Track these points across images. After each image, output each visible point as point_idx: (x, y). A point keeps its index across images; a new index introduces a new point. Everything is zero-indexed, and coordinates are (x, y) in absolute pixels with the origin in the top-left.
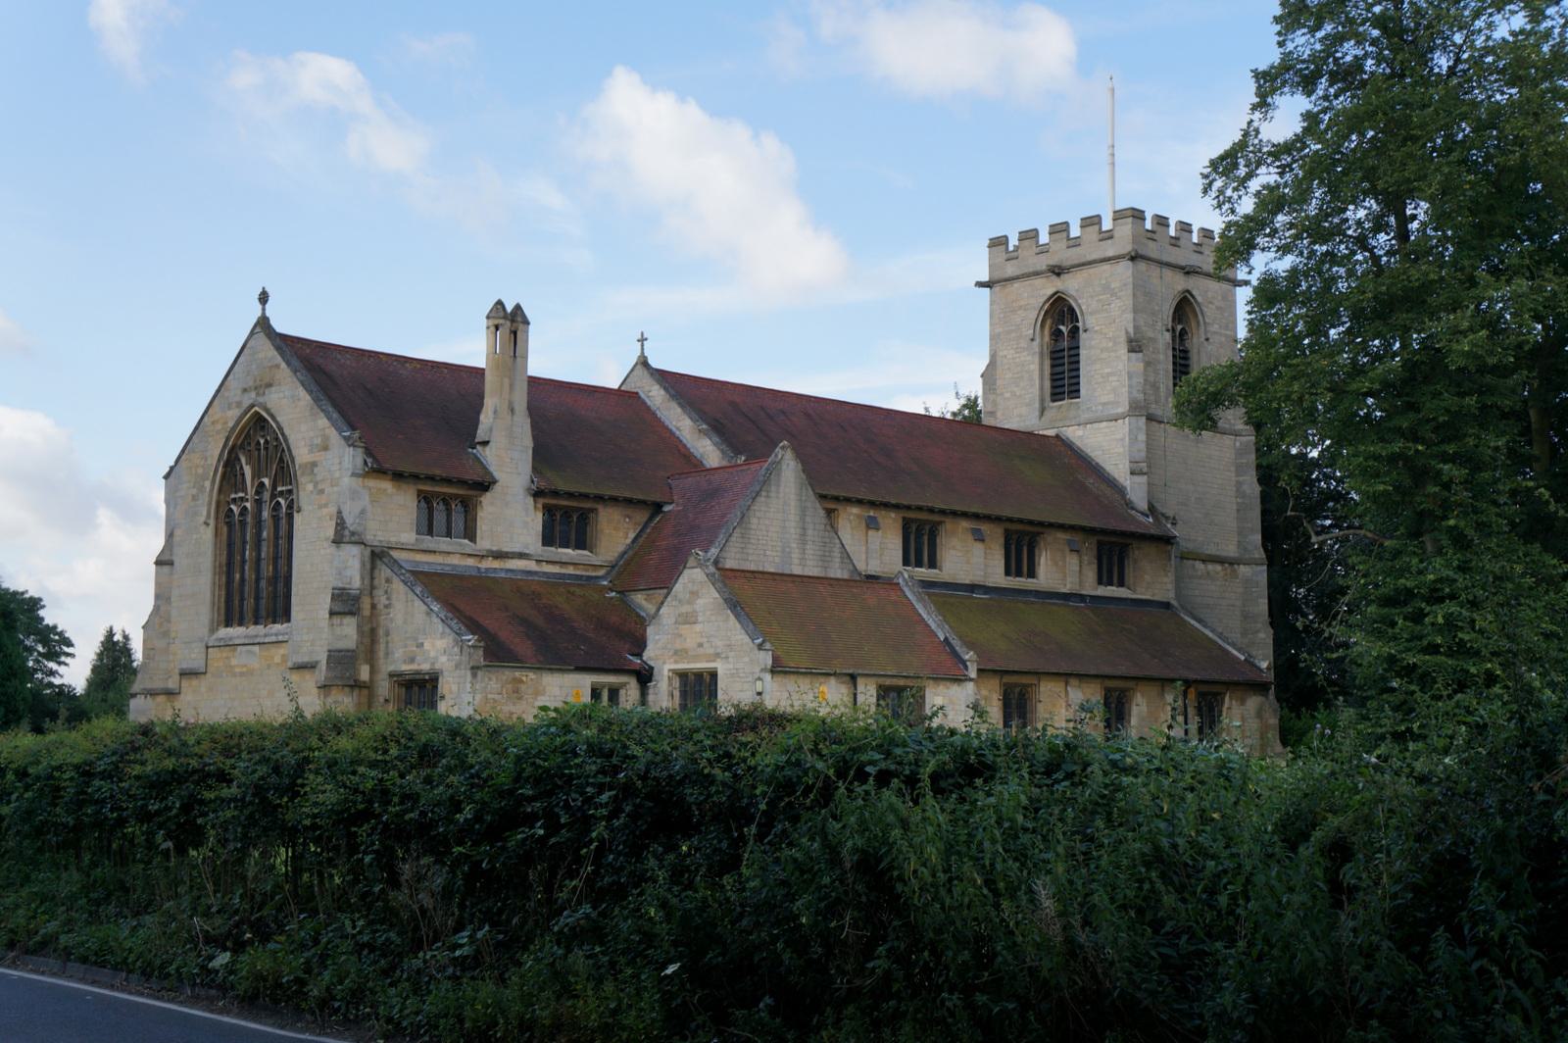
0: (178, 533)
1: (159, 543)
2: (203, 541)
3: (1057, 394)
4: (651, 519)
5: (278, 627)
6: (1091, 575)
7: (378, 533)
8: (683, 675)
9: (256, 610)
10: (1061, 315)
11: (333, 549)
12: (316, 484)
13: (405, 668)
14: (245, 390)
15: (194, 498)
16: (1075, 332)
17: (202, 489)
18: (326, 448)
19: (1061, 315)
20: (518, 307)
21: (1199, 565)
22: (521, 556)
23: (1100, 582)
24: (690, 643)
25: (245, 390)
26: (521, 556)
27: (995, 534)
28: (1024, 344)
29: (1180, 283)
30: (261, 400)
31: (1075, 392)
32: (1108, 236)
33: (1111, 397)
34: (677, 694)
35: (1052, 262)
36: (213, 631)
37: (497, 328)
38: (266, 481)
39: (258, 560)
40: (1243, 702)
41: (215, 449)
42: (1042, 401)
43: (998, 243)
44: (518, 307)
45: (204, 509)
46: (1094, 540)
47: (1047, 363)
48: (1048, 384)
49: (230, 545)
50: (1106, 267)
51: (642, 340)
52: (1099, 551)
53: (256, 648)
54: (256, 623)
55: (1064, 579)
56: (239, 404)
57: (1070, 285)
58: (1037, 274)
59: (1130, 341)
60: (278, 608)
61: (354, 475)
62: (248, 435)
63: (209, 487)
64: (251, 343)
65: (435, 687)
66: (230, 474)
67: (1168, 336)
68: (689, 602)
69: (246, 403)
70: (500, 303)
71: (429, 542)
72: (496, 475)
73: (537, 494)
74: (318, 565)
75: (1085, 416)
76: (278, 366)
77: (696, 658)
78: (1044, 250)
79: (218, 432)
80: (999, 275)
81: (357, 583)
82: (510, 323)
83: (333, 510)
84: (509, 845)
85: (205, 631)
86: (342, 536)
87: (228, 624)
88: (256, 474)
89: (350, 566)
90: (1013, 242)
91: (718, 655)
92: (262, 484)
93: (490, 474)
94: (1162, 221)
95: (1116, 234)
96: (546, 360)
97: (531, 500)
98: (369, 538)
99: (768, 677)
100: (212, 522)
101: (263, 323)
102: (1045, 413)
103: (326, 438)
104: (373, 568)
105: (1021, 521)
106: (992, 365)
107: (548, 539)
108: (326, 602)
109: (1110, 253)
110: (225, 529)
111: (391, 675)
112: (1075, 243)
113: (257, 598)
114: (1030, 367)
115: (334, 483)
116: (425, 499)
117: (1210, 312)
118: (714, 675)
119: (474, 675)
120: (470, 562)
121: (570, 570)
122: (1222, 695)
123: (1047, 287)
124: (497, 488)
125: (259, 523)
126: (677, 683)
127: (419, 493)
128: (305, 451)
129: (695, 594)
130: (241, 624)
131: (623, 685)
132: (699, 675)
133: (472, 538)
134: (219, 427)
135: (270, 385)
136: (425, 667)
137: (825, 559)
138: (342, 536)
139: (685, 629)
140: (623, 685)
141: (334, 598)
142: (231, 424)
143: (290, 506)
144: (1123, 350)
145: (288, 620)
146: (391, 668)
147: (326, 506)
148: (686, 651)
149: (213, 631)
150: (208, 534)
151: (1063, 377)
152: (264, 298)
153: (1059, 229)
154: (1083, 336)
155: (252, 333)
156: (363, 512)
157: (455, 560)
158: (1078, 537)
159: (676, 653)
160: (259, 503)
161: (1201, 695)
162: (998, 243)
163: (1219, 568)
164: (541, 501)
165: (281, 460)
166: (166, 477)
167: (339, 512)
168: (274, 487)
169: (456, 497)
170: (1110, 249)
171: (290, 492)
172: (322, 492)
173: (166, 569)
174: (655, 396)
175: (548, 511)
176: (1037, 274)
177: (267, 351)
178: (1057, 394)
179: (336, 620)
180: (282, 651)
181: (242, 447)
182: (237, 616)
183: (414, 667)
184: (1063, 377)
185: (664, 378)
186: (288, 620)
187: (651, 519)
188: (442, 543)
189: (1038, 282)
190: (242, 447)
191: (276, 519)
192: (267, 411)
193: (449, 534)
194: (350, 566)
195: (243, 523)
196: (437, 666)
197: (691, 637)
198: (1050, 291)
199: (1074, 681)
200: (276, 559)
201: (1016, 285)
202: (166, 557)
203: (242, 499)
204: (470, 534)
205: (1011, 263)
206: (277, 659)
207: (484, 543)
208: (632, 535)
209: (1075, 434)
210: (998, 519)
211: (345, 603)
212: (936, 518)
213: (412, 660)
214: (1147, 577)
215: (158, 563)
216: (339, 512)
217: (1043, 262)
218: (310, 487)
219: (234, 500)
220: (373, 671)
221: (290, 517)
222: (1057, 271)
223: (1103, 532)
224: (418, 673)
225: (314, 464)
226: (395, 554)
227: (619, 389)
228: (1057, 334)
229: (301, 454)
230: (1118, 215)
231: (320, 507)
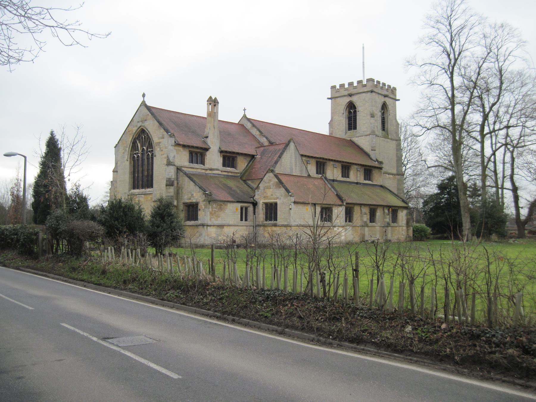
0: (119, 163)
1: (113, 166)
2: (127, 165)
3: (350, 129)
4: (251, 160)
5: (149, 189)
6: (362, 177)
7: (178, 163)
8: (266, 204)
9: (142, 184)
10: (351, 108)
11: (166, 167)
12: (160, 148)
13: (188, 201)
14: (138, 122)
15: (124, 153)
16: (355, 112)
17: (126, 150)
18: (163, 138)
19: (351, 108)
20: (216, 98)
21: (387, 175)
22: (217, 170)
23: (365, 179)
24: (269, 194)
25: (138, 122)
26: (217, 170)
27: (339, 166)
28: (340, 115)
29: (383, 99)
30: (143, 124)
31: (355, 128)
32: (365, 86)
33: (366, 130)
34: (264, 209)
35: (349, 92)
36: (129, 191)
37: (210, 104)
38: (145, 148)
39: (143, 170)
40: (402, 212)
41: (129, 139)
42: (346, 130)
43: (333, 87)
44: (216, 98)
45: (127, 156)
46: (363, 168)
47: (347, 120)
48: (347, 126)
49: (134, 166)
50: (364, 94)
51: (245, 110)
52: (365, 173)
53: (143, 196)
54: (142, 188)
55: (357, 177)
56: (136, 126)
57: (354, 99)
58: (345, 96)
59: (371, 114)
60: (150, 184)
61: (172, 145)
62: (139, 135)
63: (128, 150)
64: (140, 108)
65: (197, 207)
66: (134, 146)
67: (380, 113)
68: (268, 183)
69: (139, 126)
70: (211, 98)
71: (192, 165)
72: (211, 146)
73: (221, 152)
74: (161, 172)
75: (358, 135)
76: (148, 115)
77: (271, 199)
78: (346, 89)
79: (130, 134)
80: (334, 96)
81: (173, 177)
82: (213, 102)
83: (165, 156)
84: (123, 248)
85: (128, 191)
86: (169, 163)
87: (134, 188)
88: (142, 146)
89: (171, 172)
90: (338, 87)
91: (278, 198)
92: (143, 149)
93: (209, 146)
94: (378, 82)
95: (367, 85)
96: (222, 116)
97: (219, 154)
98: (176, 164)
99: (293, 204)
100: (129, 160)
101: (144, 104)
102: (287, 142)
103: (163, 135)
104: (177, 172)
105: (346, 162)
106: (331, 121)
107: (224, 165)
108: (165, 182)
109: (366, 91)
110: (132, 162)
111: (184, 203)
112: (355, 88)
113: (142, 181)
114: (343, 121)
115: (166, 148)
116: (191, 153)
117: (390, 107)
118: (276, 204)
119: (209, 203)
120: (203, 171)
121: (230, 174)
122: (397, 210)
123: (347, 100)
124: (210, 150)
125: (143, 160)
126: (264, 206)
127: (190, 151)
128: (157, 139)
129: (270, 180)
130: (138, 189)
131: (249, 206)
132: (271, 204)
133: (204, 165)
134: (131, 132)
135: (146, 120)
136: (194, 201)
137: (301, 171)
138: (169, 163)
139: (267, 190)
140: (249, 206)
141: (167, 181)
142: (134, 132)
143: (152, 155)
144: (369, 117)
145: (152, 187)
146: (183, 201)
147: (163, 155)
148: (267, 197)
149: (129, 191)
150: (128, 163)
151: (352, 124)
152: (144, 95)
153: (351, 84)
154: (358, 113)
155: (140, 106)
156: (174, 157)
157: (199, 171)
158: (359, 167)
159: (264, 197)
160: (142, 154)
161: (393, 210)
162: (333, 87)
163: (392, 176)
164: (222, 154)
165: (149, 142)
166: (115, 147)
167: (168, 156)
168: (147, 149)
169: (199, 152)
170: (365, 89)
171: (152, 151)
172: (162, 150)
173: (116, 173)
174: (249, 126)
175: (224, 157)
176: (345, 96)
177: (146, 111)
178: (350, 129)
179: (168, 187)
180: (151, 196)
181: (137, 138)
182: (136, 186)
183: (191, 201)
184: (352, 124)
185: (249, 120)
186: (152, 187)
187: (251, 160)
188: (196, 166)
189: (345, 98)
190: (137, 138)
191: (148, 159)
192: (145, 128)
193: (197, 163)
194: (171, 172)
195: (138, 160)
196: (198, 201)
197: (269, 192)
198: (348, 101)
199: (363, 206)
200: (148, 170)
201: (339, 99)
202: (115, 170)
203: (137, 153)
204: (203, 163)
205: (336, 93)
206: (149, 199)
207: (207, 166)
208: (246, 164)
209: (355, 140)
210: (340, 162)
211: (170, 183)
212: (325, 161)
213: (190, 199)
214: (376, 178)
215: (114, 171)
216: (168, 156)
217: (346, 93)
218: (158, 149)
219: (135, 154)
220: (178, 202)
221: (152, 158)
222: (350, 95)
223: (366, 166)
224: (191, 202)
225: (160, 143)
226: (183, 169)
227: (238, 124)
228: (350, 113)
229: (155, 139)
230: (368, 80)
231: (162, 155)
